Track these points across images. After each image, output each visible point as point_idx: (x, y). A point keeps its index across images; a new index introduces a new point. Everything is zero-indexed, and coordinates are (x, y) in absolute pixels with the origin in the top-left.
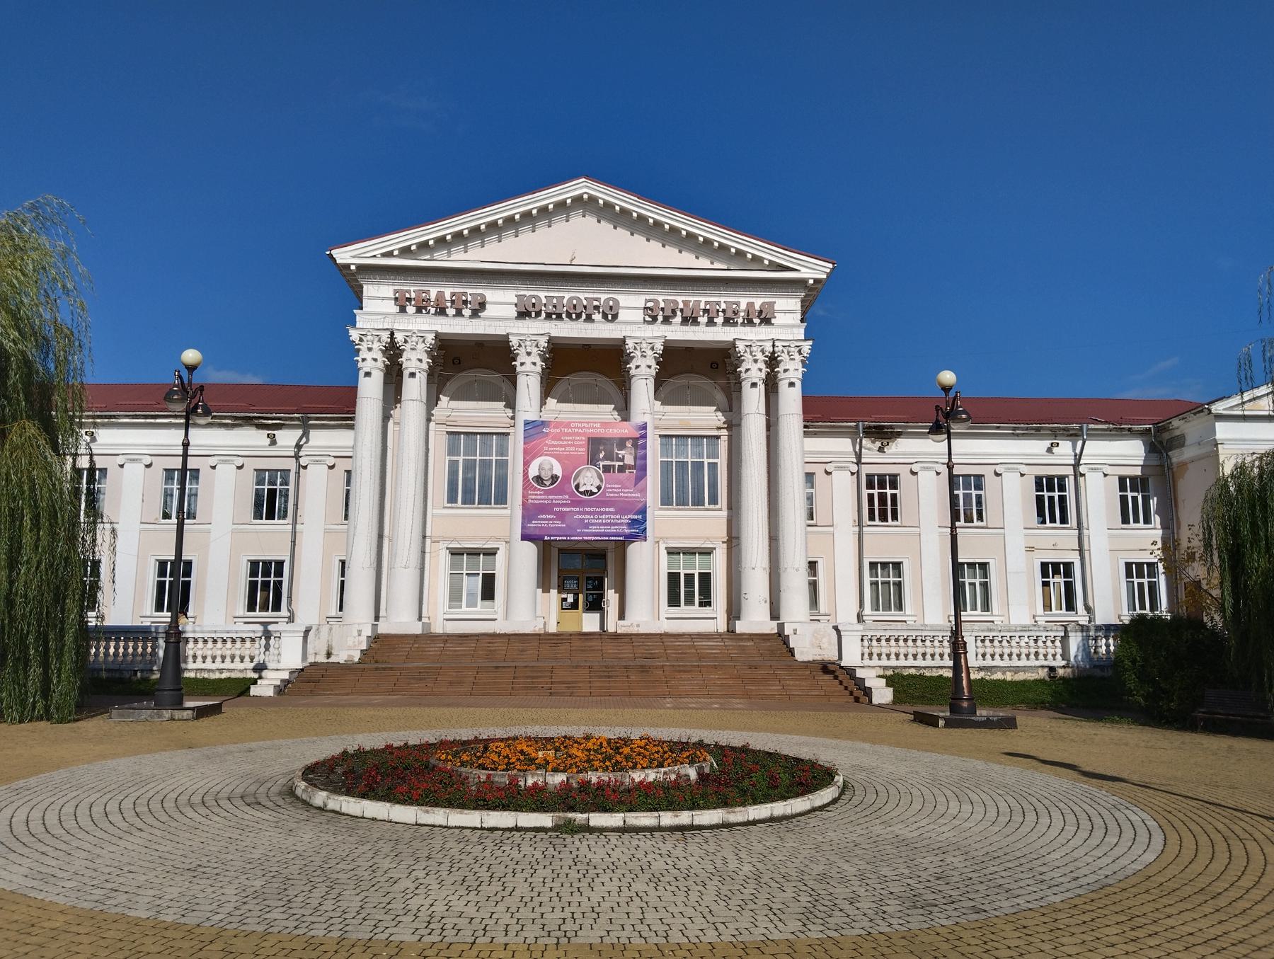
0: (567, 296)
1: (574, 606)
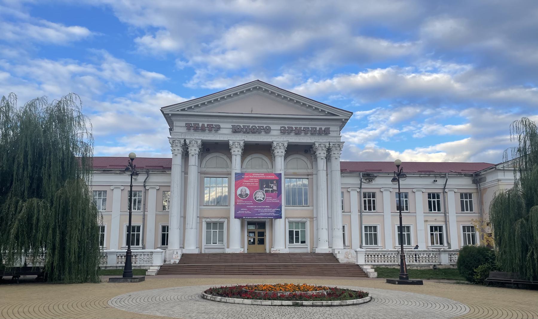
1: (254, 243)
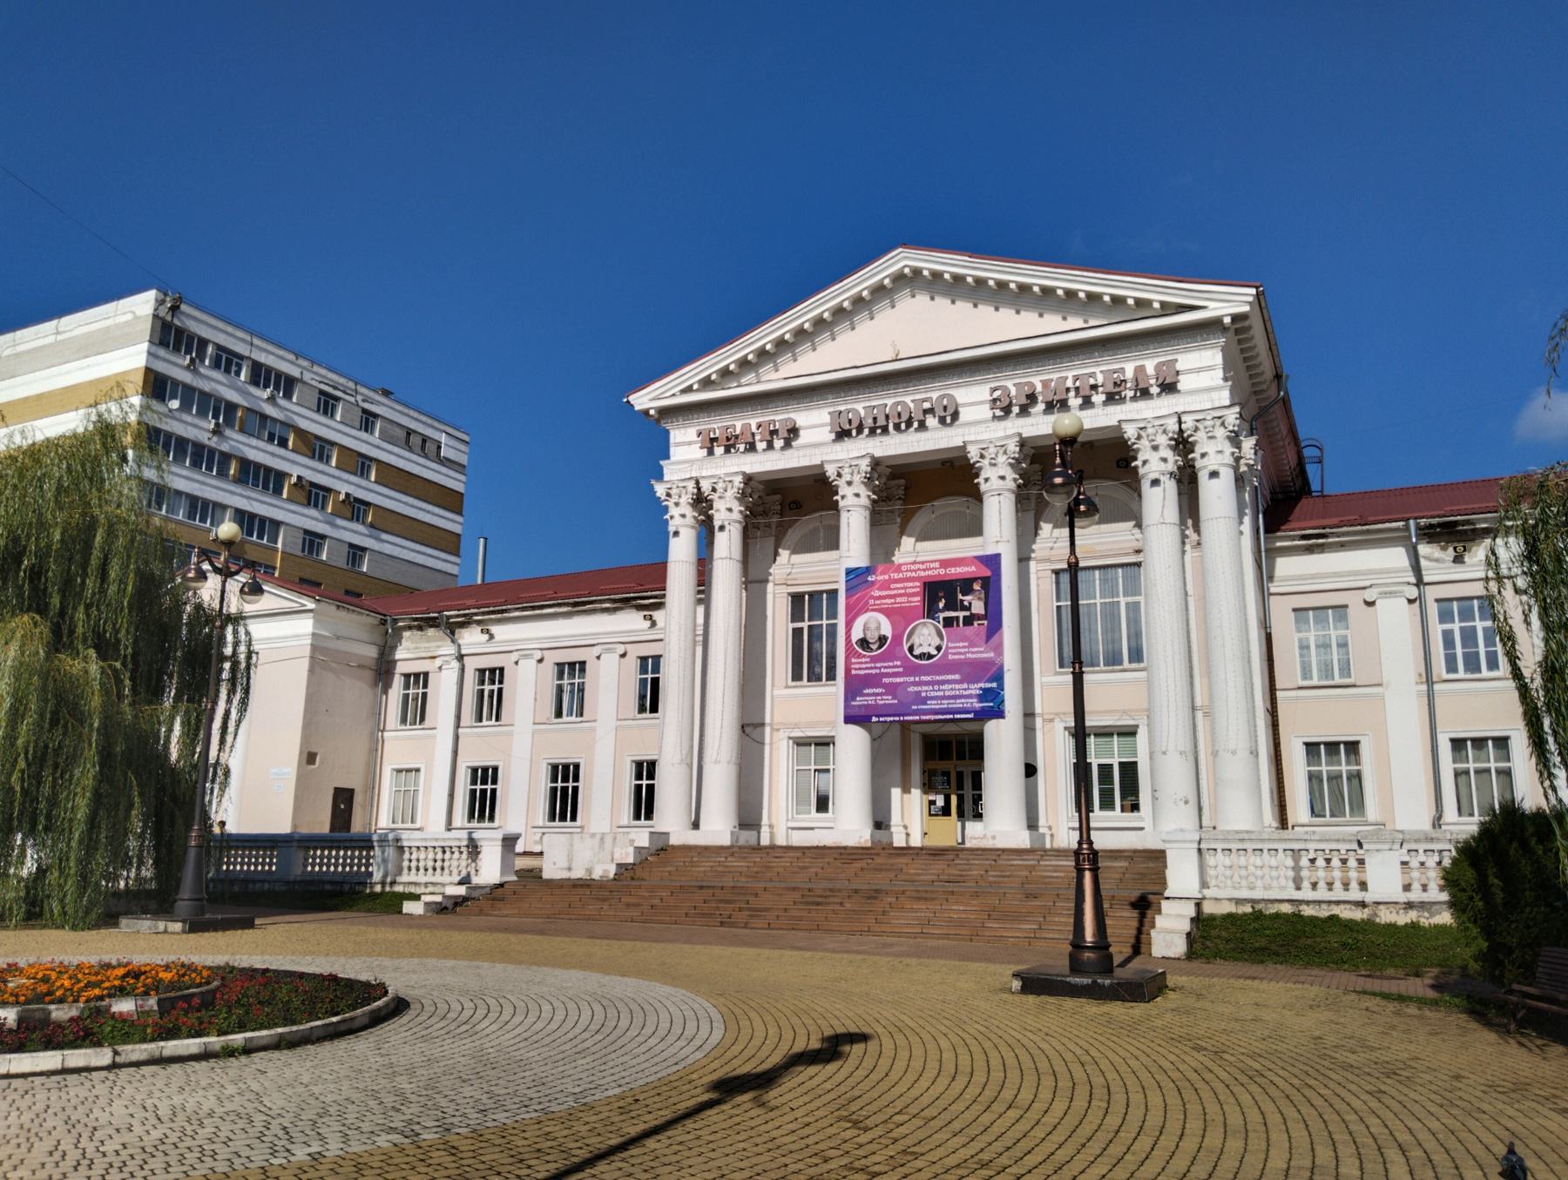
1: (946, 811)
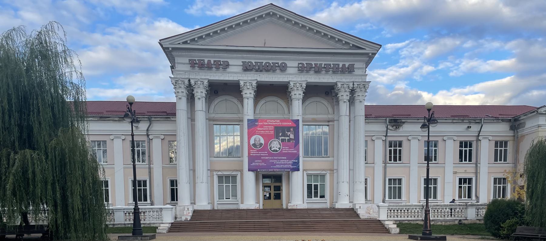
0: (264, 62)
1: (269, 198)
